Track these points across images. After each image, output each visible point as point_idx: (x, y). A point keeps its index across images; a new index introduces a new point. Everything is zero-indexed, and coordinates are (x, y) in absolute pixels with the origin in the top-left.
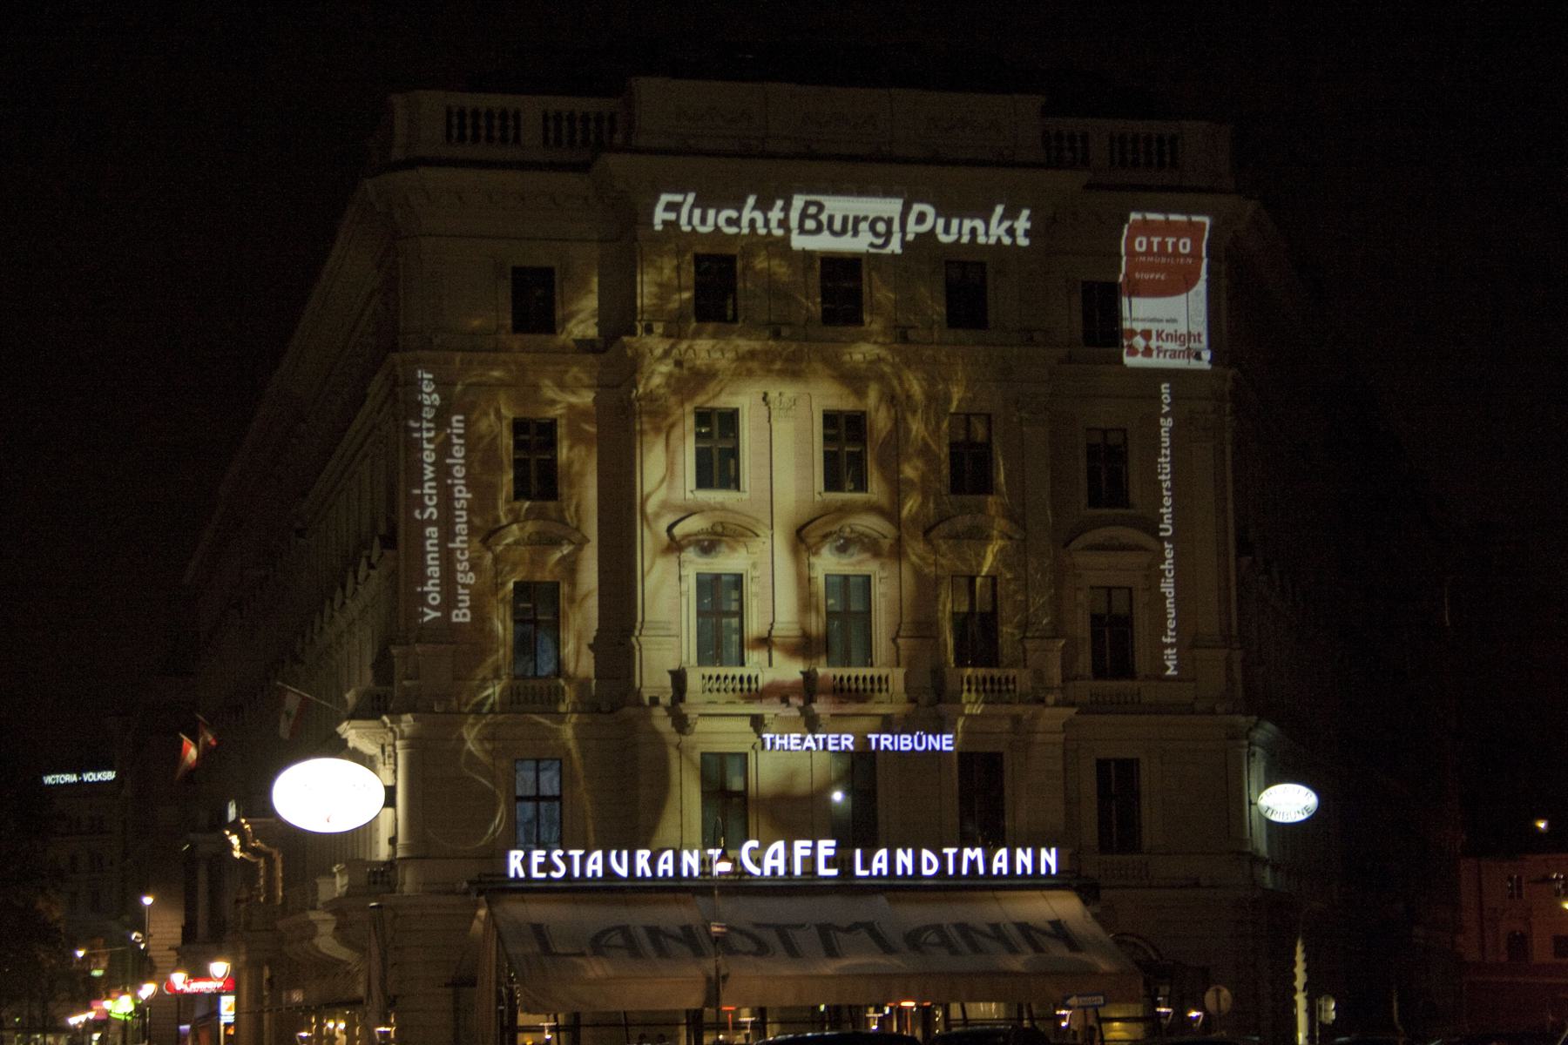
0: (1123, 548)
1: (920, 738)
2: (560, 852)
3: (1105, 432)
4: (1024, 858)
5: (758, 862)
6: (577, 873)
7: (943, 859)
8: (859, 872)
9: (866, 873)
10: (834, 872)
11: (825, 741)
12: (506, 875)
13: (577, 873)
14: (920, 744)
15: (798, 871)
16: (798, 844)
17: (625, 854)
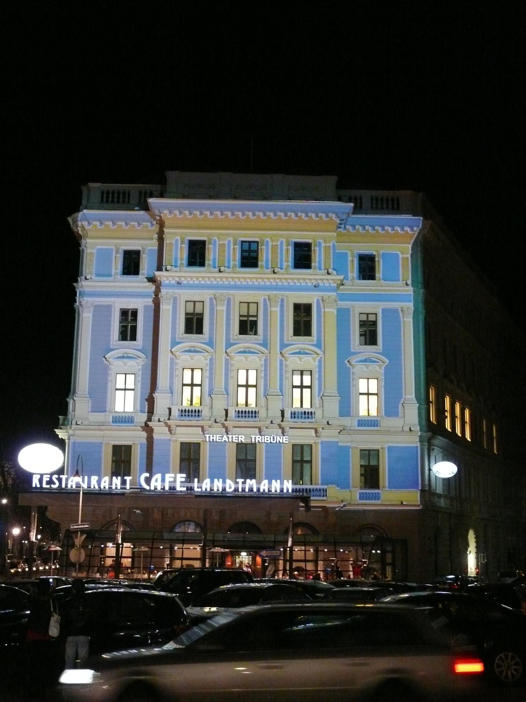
1: (274, 438)
2: (57, 476)
3: (367, 314)
5: (149, 485)
6: (63, 486)
8: (196, 489)
12: (32, 486)
13: (63, 486)
15: (167, 488)
16: (167, 476)
17: (86, 477)
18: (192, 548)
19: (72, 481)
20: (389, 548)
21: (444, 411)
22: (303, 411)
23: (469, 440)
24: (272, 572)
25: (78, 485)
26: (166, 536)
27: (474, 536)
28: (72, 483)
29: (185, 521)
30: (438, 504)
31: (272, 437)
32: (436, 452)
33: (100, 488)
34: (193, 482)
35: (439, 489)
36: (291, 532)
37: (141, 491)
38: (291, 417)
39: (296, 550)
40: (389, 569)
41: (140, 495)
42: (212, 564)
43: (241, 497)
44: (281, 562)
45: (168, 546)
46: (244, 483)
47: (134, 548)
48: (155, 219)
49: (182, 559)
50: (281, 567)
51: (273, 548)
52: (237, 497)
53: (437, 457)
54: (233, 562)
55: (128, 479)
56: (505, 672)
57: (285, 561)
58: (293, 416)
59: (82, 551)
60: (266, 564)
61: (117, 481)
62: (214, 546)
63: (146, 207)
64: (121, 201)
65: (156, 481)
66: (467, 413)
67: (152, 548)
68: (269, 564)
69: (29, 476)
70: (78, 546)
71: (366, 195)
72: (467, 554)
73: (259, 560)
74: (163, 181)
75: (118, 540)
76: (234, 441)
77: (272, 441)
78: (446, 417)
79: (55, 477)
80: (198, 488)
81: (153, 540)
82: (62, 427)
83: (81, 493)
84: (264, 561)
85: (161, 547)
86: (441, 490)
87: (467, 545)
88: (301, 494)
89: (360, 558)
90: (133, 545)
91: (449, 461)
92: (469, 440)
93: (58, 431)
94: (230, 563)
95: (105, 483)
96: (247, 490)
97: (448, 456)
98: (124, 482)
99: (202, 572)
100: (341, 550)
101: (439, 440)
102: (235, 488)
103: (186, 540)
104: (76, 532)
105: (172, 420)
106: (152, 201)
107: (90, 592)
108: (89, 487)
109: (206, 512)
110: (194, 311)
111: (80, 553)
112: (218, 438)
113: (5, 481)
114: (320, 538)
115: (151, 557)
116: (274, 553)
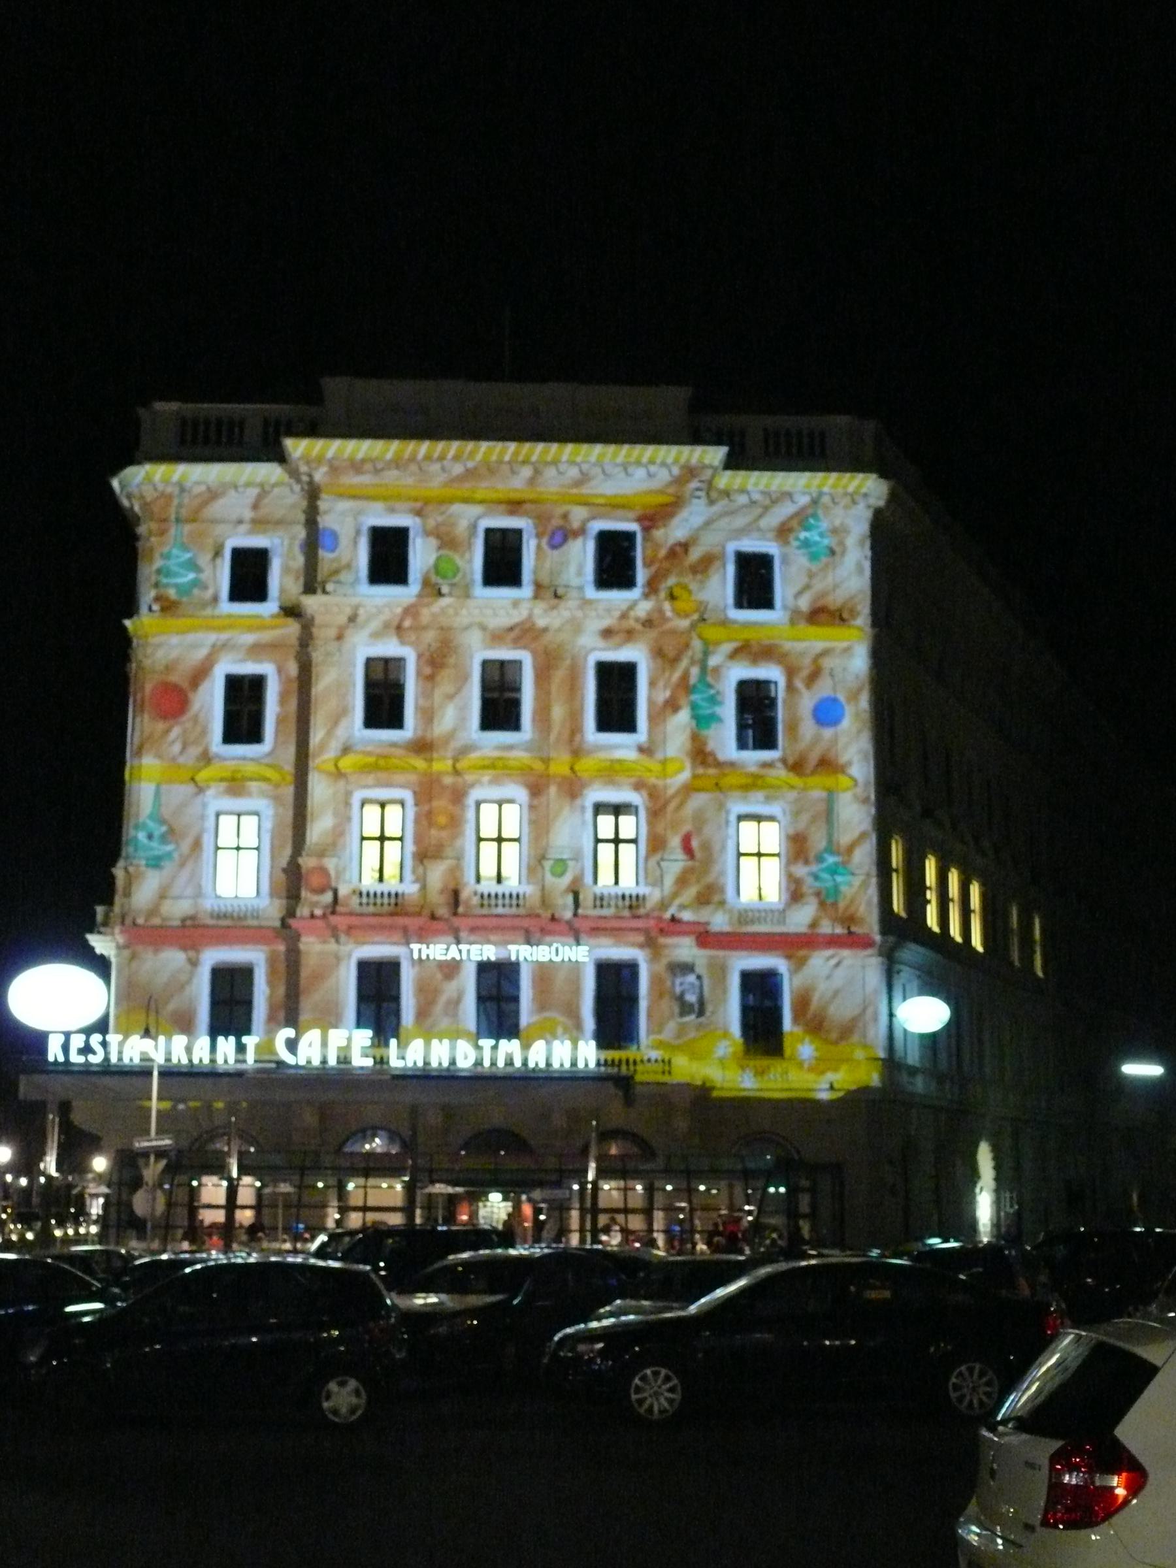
12: (47, 1060)
20: (805, 1183)
21: (923, 888)
22: (620, 893)
25: (146, 1058)
26: (327, 1160)
30: (910, 1088)
32: (905, 975)
35: (913, 1057)
36: (593, 1151)
37: (278, 1068)
38: (595, 907)
41: (274, 1077)
42: (430, 1218)
44: (575, 1214)
45: (333, 1181)
48: (298, 481)
49: (365, 1209)
51: (558, 1184)
53: (908, 987)
54: (474, 1215)
56: (968, 1398)
57: (582, 1210)
58: (598, 903)
59: (159, 1193)
61: (226, 1046)
63: (280, 457)
64: (224, 440)
66: (975, 890)
67: (300, 1187)
68: (548, 1217)
69: (39, 1040)
71: (755, 424)
74: (315, 397)
75: (229, 1172)
81: (303, 1170)
83: (155, 1073)
84: (537, 1211)
87: (973, 1175)
88: (616, 1070)
92: (980, 949)
95: (201, 1052)
97: (932, 985)
98: (241, 1048)
99: (408, 1232)
101: (912, 952)
103: (373, 1167)
104: (145, 1154)
105: (341, 914)
106: (289, 443)
108: (168, 1060)
111: (154, 1199)
114: (660, 1163)
116: (559, 1193)
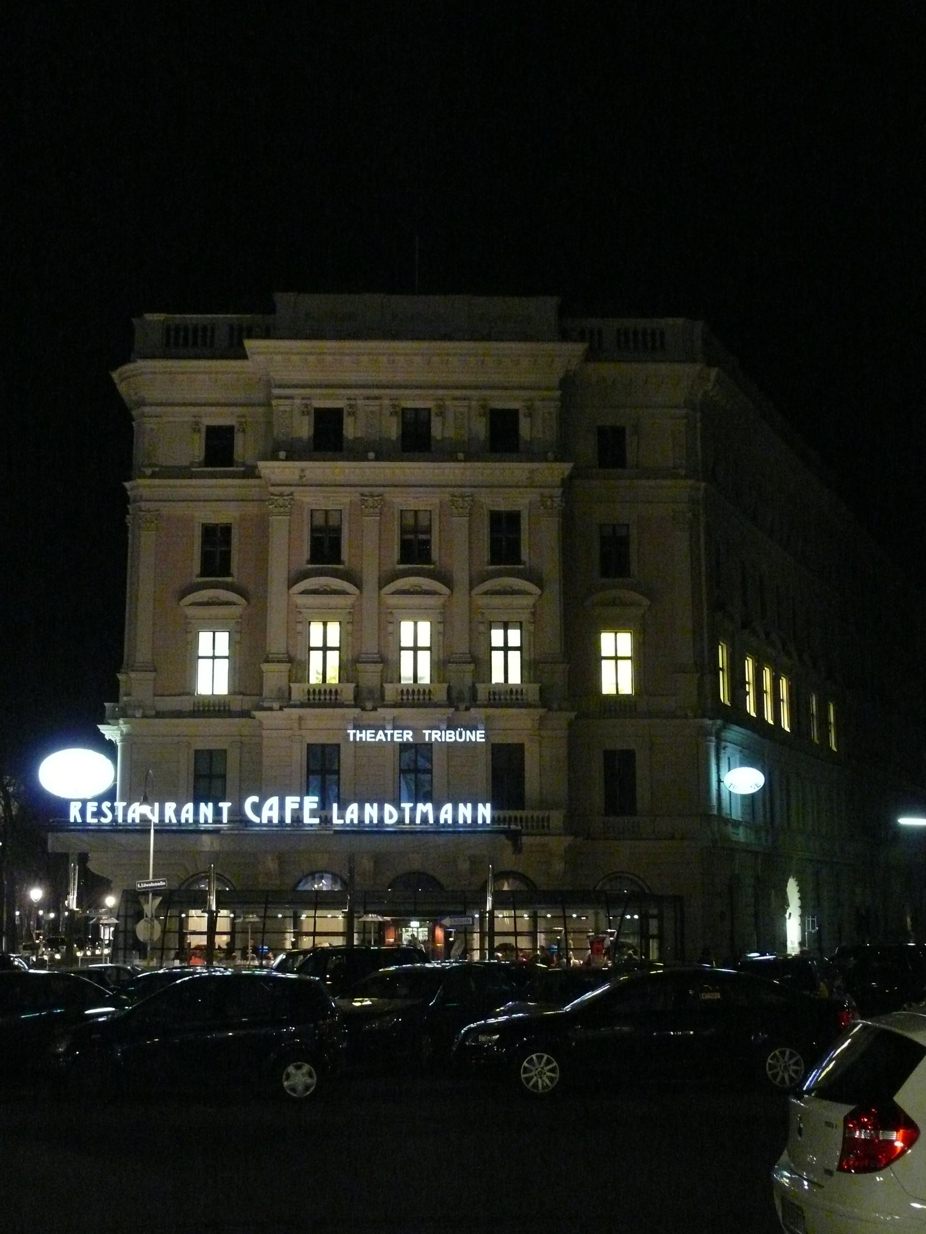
0: (514, 592)
4: (465, 811)
7: (401, 810)
8: (336, 821)
9: (341, 822)
10: (316, 821)
11: (392, 735)
13: (120, 820)
14: (461, 737)
15: (288, 820)
17: (157, 805)
18: (329, 916)
19: (134, 812)
21: (744, 683)
23: (788, 730)
24: (459, 952)
27: (797, 889)
28: (134, 815)
29: (316, 874)
30: (735, 838)
31: (457, 732)
33: (179, 821)
34: (331, 808)
36: (490, 888)
39: (501, 916)
40: (654, 944)
43: (407, 832)
45: (290, 913)
46: (413, 810)
47: (234, 919)
49: (314, 934)
50: (476, 945)
51: (463, 914)
52: (403, 832)
54: (399, 938)
55: (225, 806)
57: (482, 935)
59: (156, 922)
60: (451, 939)
61: (207, 810)
62: (367, 913)
65: (271, 808)
66: (784, 684)
67: (265, 917)
69: (62, 806)
70: (150, 916)
72: (785, 919)
73: (439, 933)
75: (210, 906)
76: (396, 740)
77: (458, 740)
78: (748, 693)
79: (106, 805)
80: (338, 818)
82: (110, 721)
83: (152, 831)
84: (447, 935)
85: (280, 916)
86: (740, 814)
87: (784, 903)
89: (602, 928)
90: (234, 912)
91: (752, 766)
92: (788, 730)
93: (103, 728)
94: (392, 940)
96: (418, 821)
97: (751, 758)
98: (218, 812)
99: (348, 951)
100: (574, 916)
102: (399, 818)
103: (320, 901)
104: (145, 893)
107: (187, 979)
109: (351, 858)
110: (326, 521)
111: (152, 927)
112: (369, 735)
113: (7, 808)
115: (264, 932)
116: (464, 921)
